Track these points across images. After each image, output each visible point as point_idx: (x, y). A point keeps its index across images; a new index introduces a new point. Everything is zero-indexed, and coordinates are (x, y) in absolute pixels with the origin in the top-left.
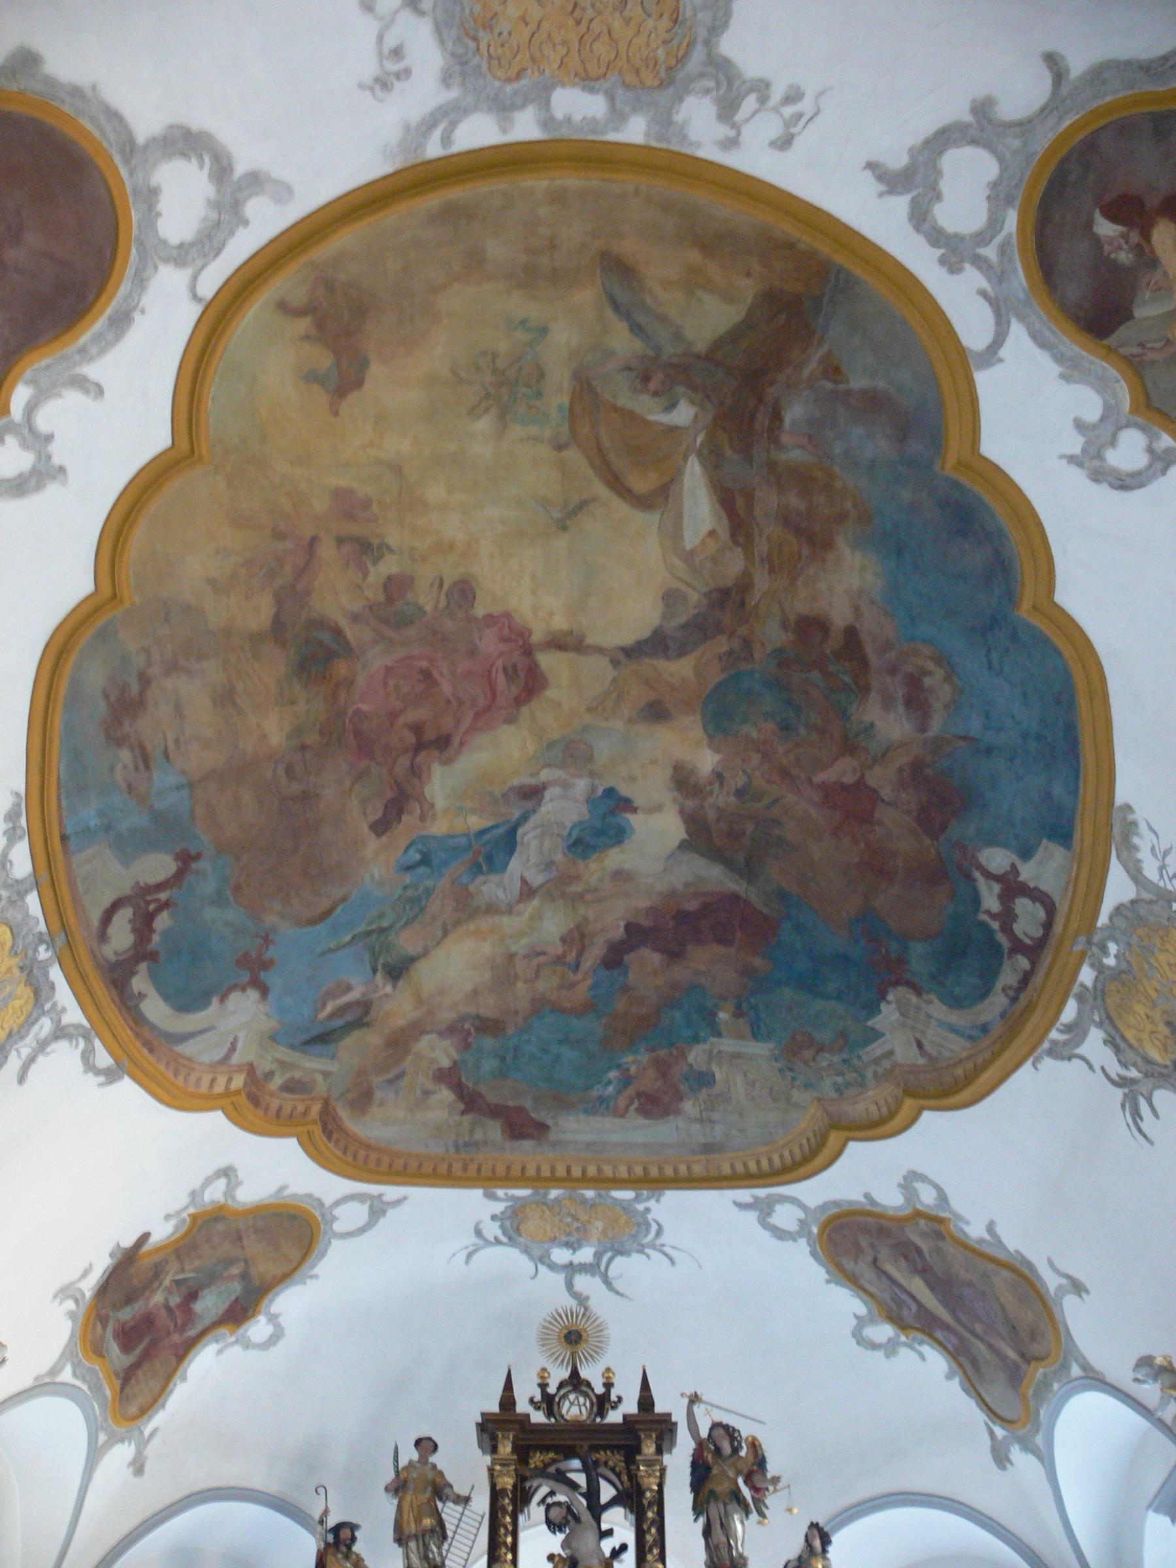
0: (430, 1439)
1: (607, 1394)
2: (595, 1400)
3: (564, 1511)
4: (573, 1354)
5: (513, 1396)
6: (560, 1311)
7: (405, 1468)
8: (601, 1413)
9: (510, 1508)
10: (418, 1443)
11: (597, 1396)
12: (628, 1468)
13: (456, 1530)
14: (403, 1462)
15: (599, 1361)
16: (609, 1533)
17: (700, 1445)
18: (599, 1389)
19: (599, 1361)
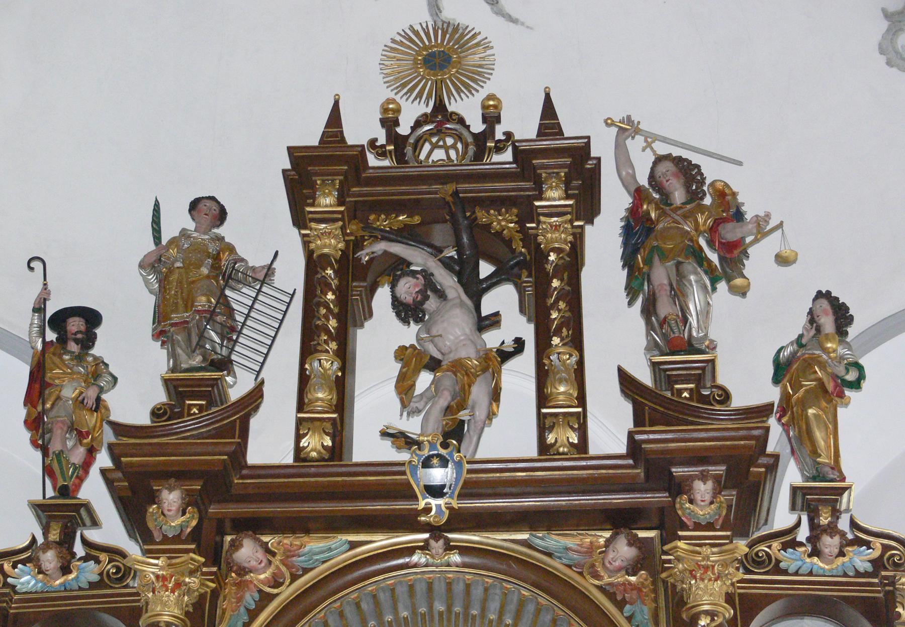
0: (212, 199)
1: (489, 133)
2: (470, 139)
3: (421, 280)
4: (438, 86)
5: (342, 132)
6: (417, 27)
7: (173, 241)
8: (478, 157)
9: (334, 283)
10: (194, 206)
11: (475, 136)
12: (523, 230)
13: (250, 311)
14: (169, 232)
15: (477, 91)
16: (494, 321)
17: (639, 194)
18: (478, 126)
19: (477, 91)
